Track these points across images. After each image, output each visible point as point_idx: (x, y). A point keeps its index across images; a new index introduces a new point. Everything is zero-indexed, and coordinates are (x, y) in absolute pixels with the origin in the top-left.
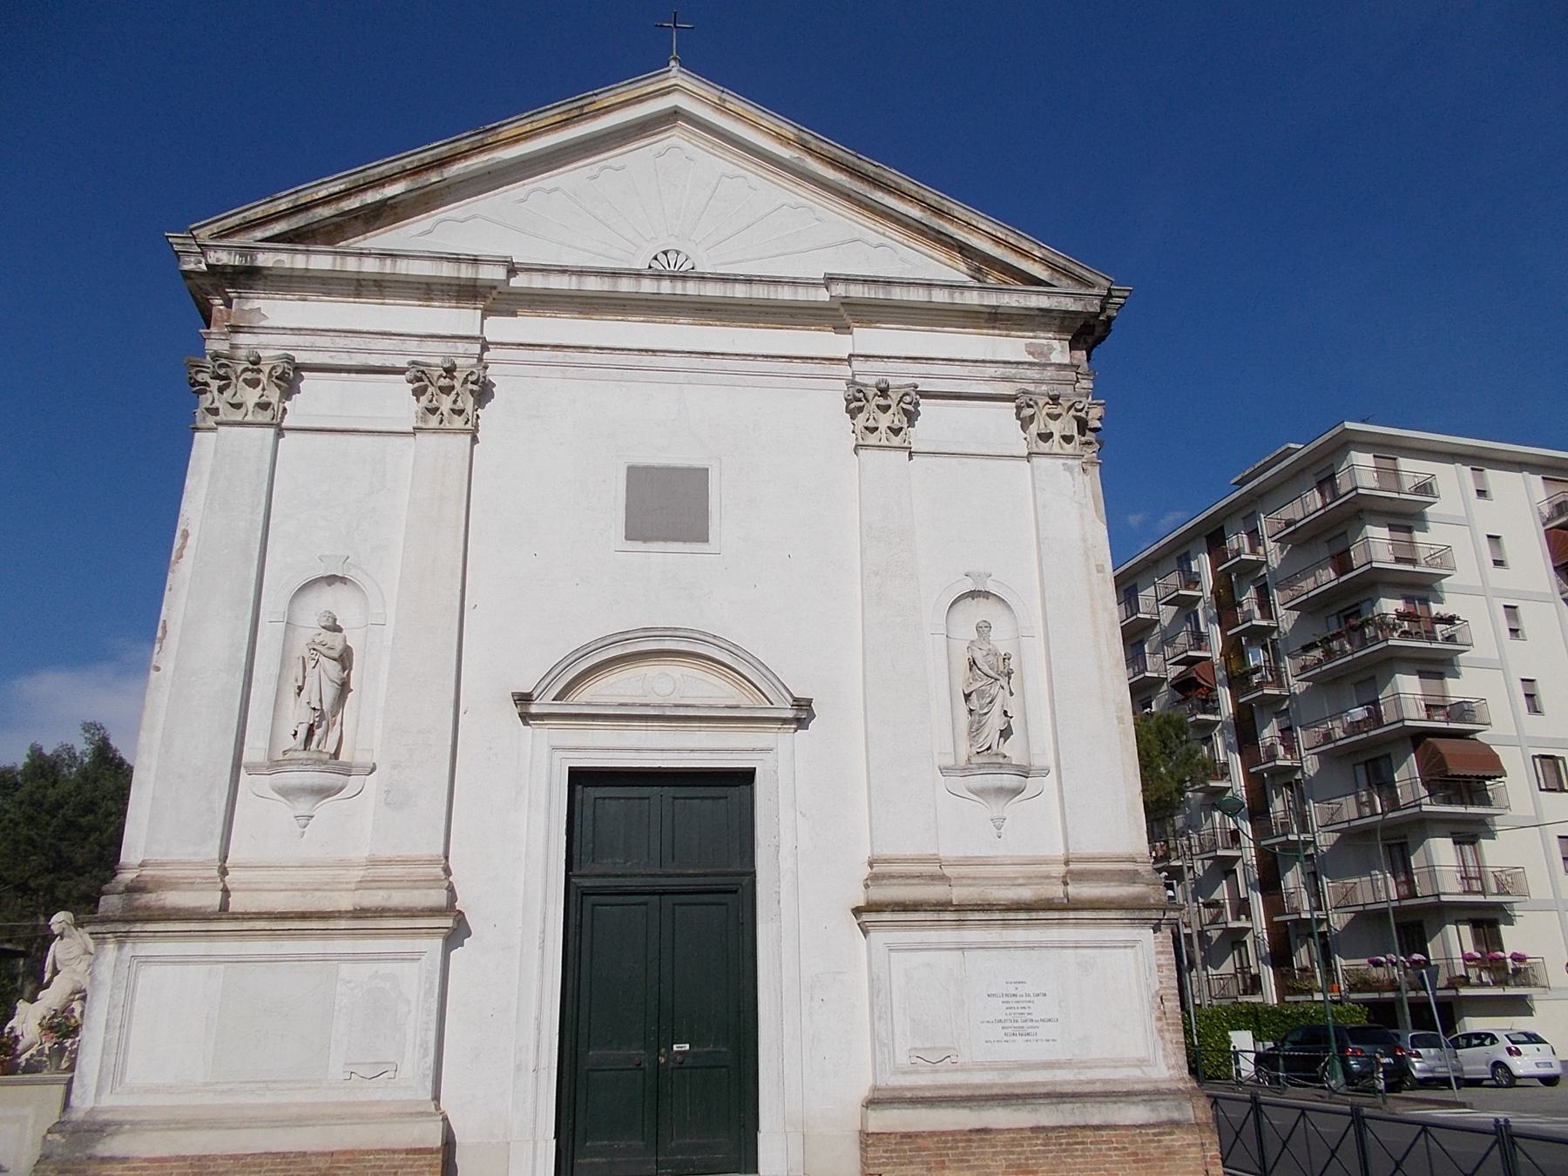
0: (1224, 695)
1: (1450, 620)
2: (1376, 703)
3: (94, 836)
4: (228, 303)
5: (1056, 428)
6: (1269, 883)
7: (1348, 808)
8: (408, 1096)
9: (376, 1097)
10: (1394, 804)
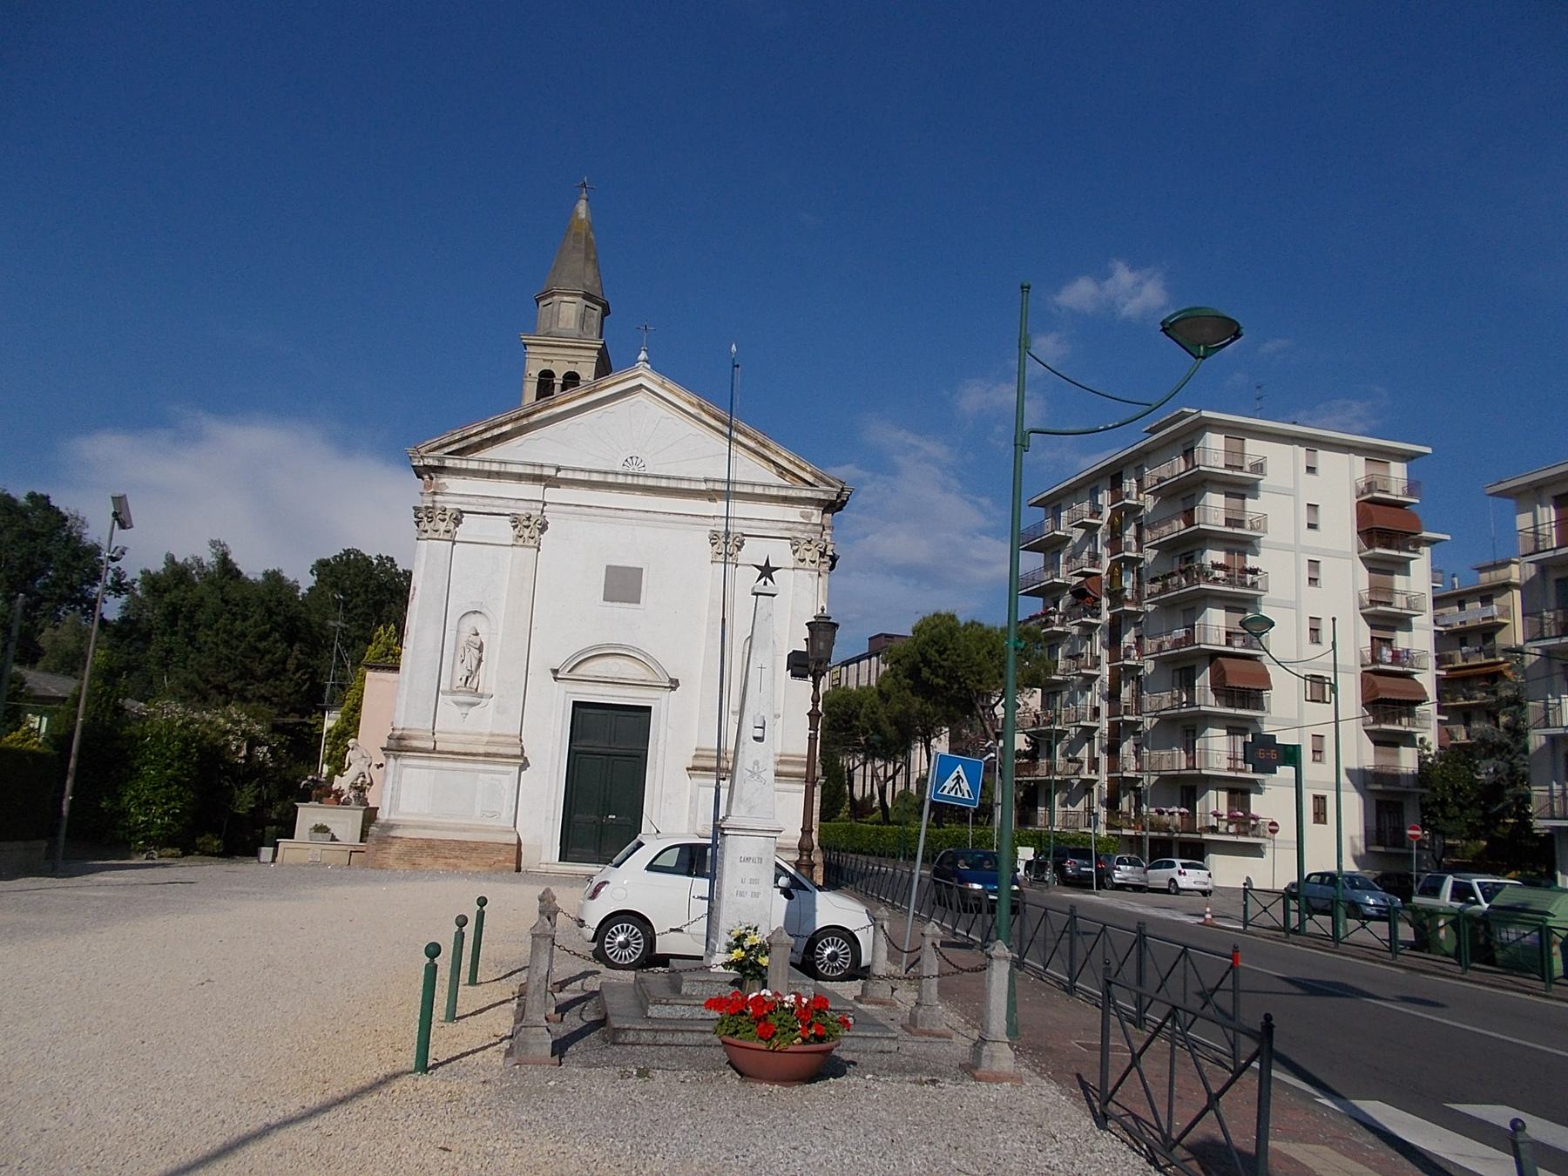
0: (1105, 602)
1: (1254, 571)
2: (1193, 627)
3: (267, 657)
4: (431, 478)
5: (808, 556)
6: (1113, 750)
7: (1165, 699)
8: (505, 825)
9: (493, 824)
10: (1191, 702)
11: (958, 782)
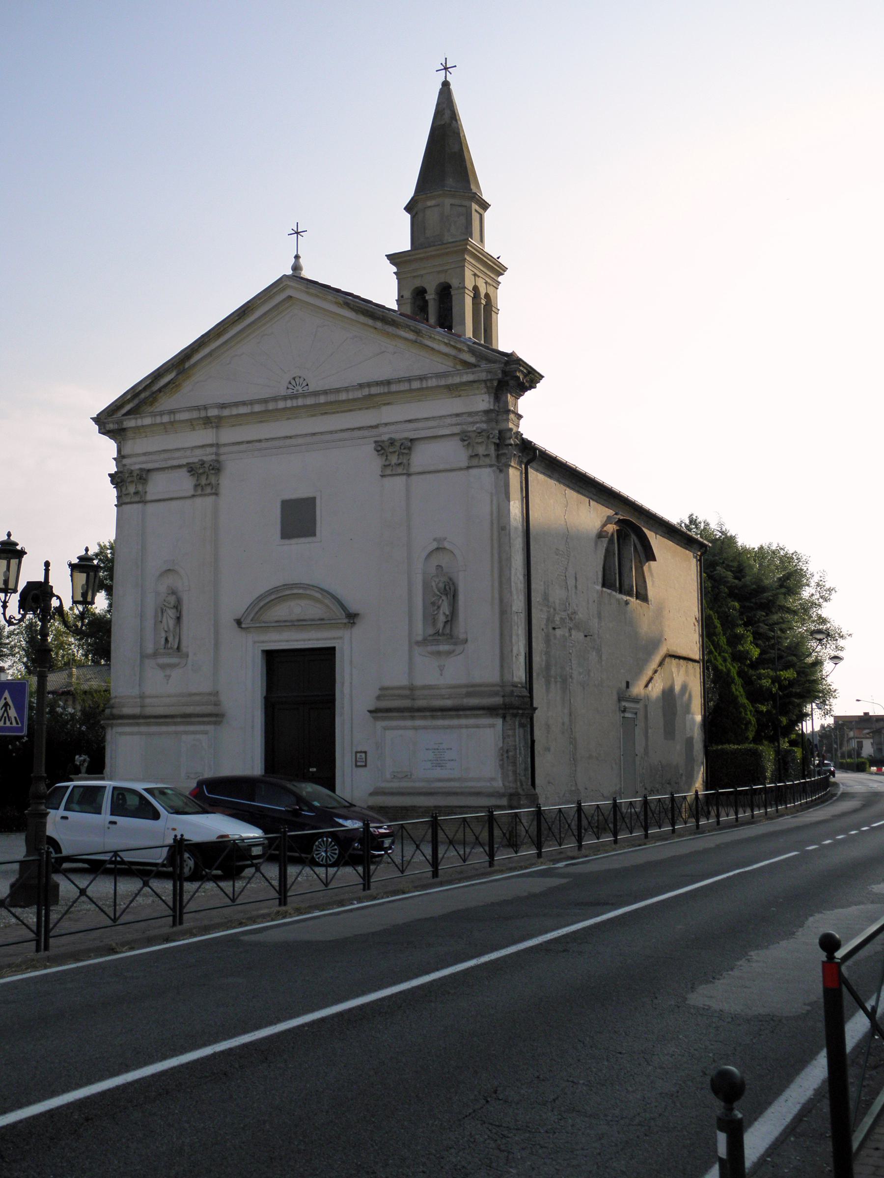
11: (6, 710)
